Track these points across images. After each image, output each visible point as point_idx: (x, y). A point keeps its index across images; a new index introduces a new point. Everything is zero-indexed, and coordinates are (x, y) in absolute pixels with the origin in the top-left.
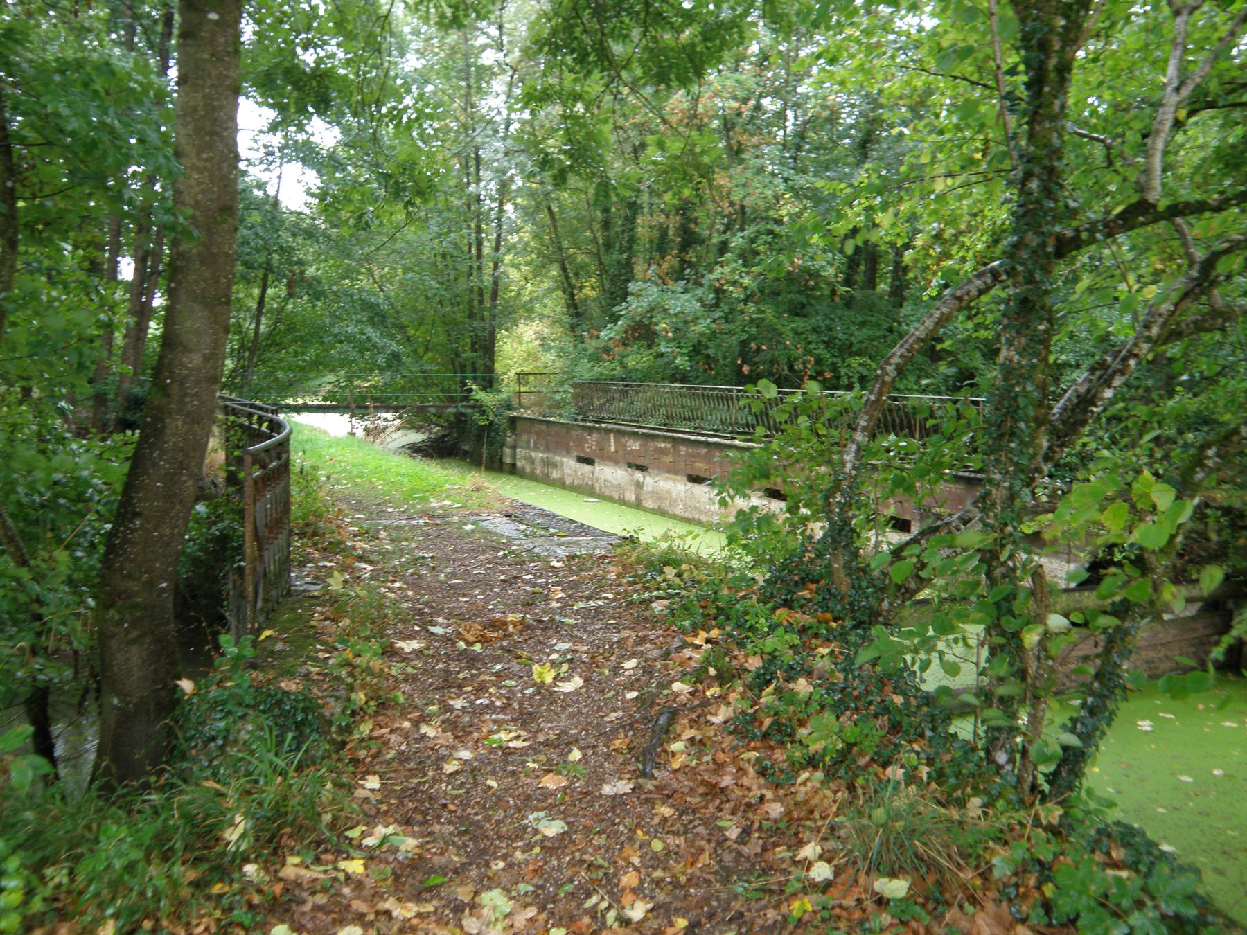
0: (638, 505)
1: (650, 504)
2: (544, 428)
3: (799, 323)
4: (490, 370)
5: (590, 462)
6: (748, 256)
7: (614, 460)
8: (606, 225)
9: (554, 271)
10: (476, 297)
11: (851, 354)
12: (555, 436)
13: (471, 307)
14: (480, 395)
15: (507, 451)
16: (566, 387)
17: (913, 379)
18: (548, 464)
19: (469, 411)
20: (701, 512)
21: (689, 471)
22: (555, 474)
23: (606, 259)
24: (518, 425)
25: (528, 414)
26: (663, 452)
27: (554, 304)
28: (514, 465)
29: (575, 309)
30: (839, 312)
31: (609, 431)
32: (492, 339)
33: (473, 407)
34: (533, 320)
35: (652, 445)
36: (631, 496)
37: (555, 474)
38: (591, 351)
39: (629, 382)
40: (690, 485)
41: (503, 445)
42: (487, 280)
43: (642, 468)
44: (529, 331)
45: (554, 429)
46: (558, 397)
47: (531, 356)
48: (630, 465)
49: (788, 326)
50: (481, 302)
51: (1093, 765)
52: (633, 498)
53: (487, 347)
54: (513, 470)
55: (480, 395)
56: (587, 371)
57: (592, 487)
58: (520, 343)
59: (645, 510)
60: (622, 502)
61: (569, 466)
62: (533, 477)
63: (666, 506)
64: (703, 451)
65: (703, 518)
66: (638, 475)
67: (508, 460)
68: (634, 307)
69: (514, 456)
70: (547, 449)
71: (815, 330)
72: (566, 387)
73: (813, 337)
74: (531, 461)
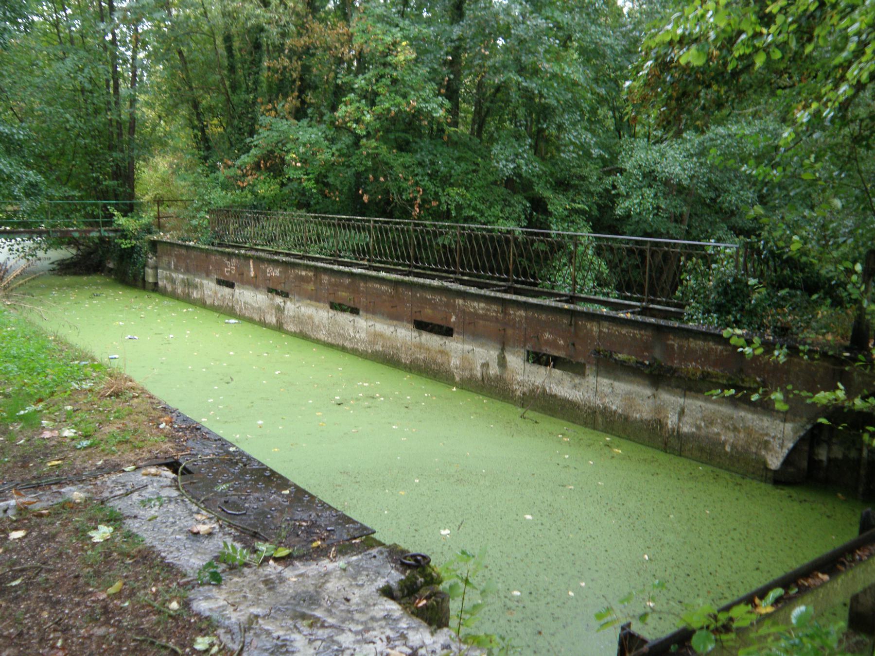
0: (279, 327)
1: (291, 328)
2: (184, 251)
3: (407, 159)
4: (132, 196)
5: (231, 285)
6: (371, 97)
7: (253, 284)
8: (232, 69)
9: (184, 111)
10: (116, 131)
11: (452, 185)
12: (195, 261)
13: (111, 139)
14: (121, 221)
15: (149, 271)
16: (203, 214)
17: (499, 207)
18: (188, 284)
19: (112, 235)
20: (343, 337)
21: (332, 299)
22: (195, 295)
23: (235, 99)
24: (159, 248)
25: (167, 237)
26: (303, 279)
27: (184, 138)
28: (156, 284)
29: (204, 143)
30: (440, 149)
31: (247, 258)
32: (131, 168)
33: (116, 231)
34: (166, 152)
35: (292, 272)
36: (272, 319)
37: (195, 295)
38: (221, 179)
39: (262, 208)
40: (332, 313)
41: (145, 265)
42: (125, 117)
43: (285, 295)
44: (162, 163)
45: (193, 254)
46: (194, 222)
47: (164, 181)
48: (270, 290)
49: (398, 161)
50: (120, 135)
51: (366, 320)
52: (274, 320)
53: (126, 176)
54: (155, 288)
55: (121, 221)
56: (219, 197)
57: (233, 308)
58: (156, 171)
59: (287, 333)
60: (263, 324)
61: (209, 288)
62: (174, 296)
63: (307, 330)
64: (347, 281)
65: (347, 344)
66: (279, 300)
67: (150, 279)
68: (262, 140)
69: (156, 275)
70: (187, 271)
71: (420, 164)
72: (203, 214)
73: (419, 170)
74: (173, 281)
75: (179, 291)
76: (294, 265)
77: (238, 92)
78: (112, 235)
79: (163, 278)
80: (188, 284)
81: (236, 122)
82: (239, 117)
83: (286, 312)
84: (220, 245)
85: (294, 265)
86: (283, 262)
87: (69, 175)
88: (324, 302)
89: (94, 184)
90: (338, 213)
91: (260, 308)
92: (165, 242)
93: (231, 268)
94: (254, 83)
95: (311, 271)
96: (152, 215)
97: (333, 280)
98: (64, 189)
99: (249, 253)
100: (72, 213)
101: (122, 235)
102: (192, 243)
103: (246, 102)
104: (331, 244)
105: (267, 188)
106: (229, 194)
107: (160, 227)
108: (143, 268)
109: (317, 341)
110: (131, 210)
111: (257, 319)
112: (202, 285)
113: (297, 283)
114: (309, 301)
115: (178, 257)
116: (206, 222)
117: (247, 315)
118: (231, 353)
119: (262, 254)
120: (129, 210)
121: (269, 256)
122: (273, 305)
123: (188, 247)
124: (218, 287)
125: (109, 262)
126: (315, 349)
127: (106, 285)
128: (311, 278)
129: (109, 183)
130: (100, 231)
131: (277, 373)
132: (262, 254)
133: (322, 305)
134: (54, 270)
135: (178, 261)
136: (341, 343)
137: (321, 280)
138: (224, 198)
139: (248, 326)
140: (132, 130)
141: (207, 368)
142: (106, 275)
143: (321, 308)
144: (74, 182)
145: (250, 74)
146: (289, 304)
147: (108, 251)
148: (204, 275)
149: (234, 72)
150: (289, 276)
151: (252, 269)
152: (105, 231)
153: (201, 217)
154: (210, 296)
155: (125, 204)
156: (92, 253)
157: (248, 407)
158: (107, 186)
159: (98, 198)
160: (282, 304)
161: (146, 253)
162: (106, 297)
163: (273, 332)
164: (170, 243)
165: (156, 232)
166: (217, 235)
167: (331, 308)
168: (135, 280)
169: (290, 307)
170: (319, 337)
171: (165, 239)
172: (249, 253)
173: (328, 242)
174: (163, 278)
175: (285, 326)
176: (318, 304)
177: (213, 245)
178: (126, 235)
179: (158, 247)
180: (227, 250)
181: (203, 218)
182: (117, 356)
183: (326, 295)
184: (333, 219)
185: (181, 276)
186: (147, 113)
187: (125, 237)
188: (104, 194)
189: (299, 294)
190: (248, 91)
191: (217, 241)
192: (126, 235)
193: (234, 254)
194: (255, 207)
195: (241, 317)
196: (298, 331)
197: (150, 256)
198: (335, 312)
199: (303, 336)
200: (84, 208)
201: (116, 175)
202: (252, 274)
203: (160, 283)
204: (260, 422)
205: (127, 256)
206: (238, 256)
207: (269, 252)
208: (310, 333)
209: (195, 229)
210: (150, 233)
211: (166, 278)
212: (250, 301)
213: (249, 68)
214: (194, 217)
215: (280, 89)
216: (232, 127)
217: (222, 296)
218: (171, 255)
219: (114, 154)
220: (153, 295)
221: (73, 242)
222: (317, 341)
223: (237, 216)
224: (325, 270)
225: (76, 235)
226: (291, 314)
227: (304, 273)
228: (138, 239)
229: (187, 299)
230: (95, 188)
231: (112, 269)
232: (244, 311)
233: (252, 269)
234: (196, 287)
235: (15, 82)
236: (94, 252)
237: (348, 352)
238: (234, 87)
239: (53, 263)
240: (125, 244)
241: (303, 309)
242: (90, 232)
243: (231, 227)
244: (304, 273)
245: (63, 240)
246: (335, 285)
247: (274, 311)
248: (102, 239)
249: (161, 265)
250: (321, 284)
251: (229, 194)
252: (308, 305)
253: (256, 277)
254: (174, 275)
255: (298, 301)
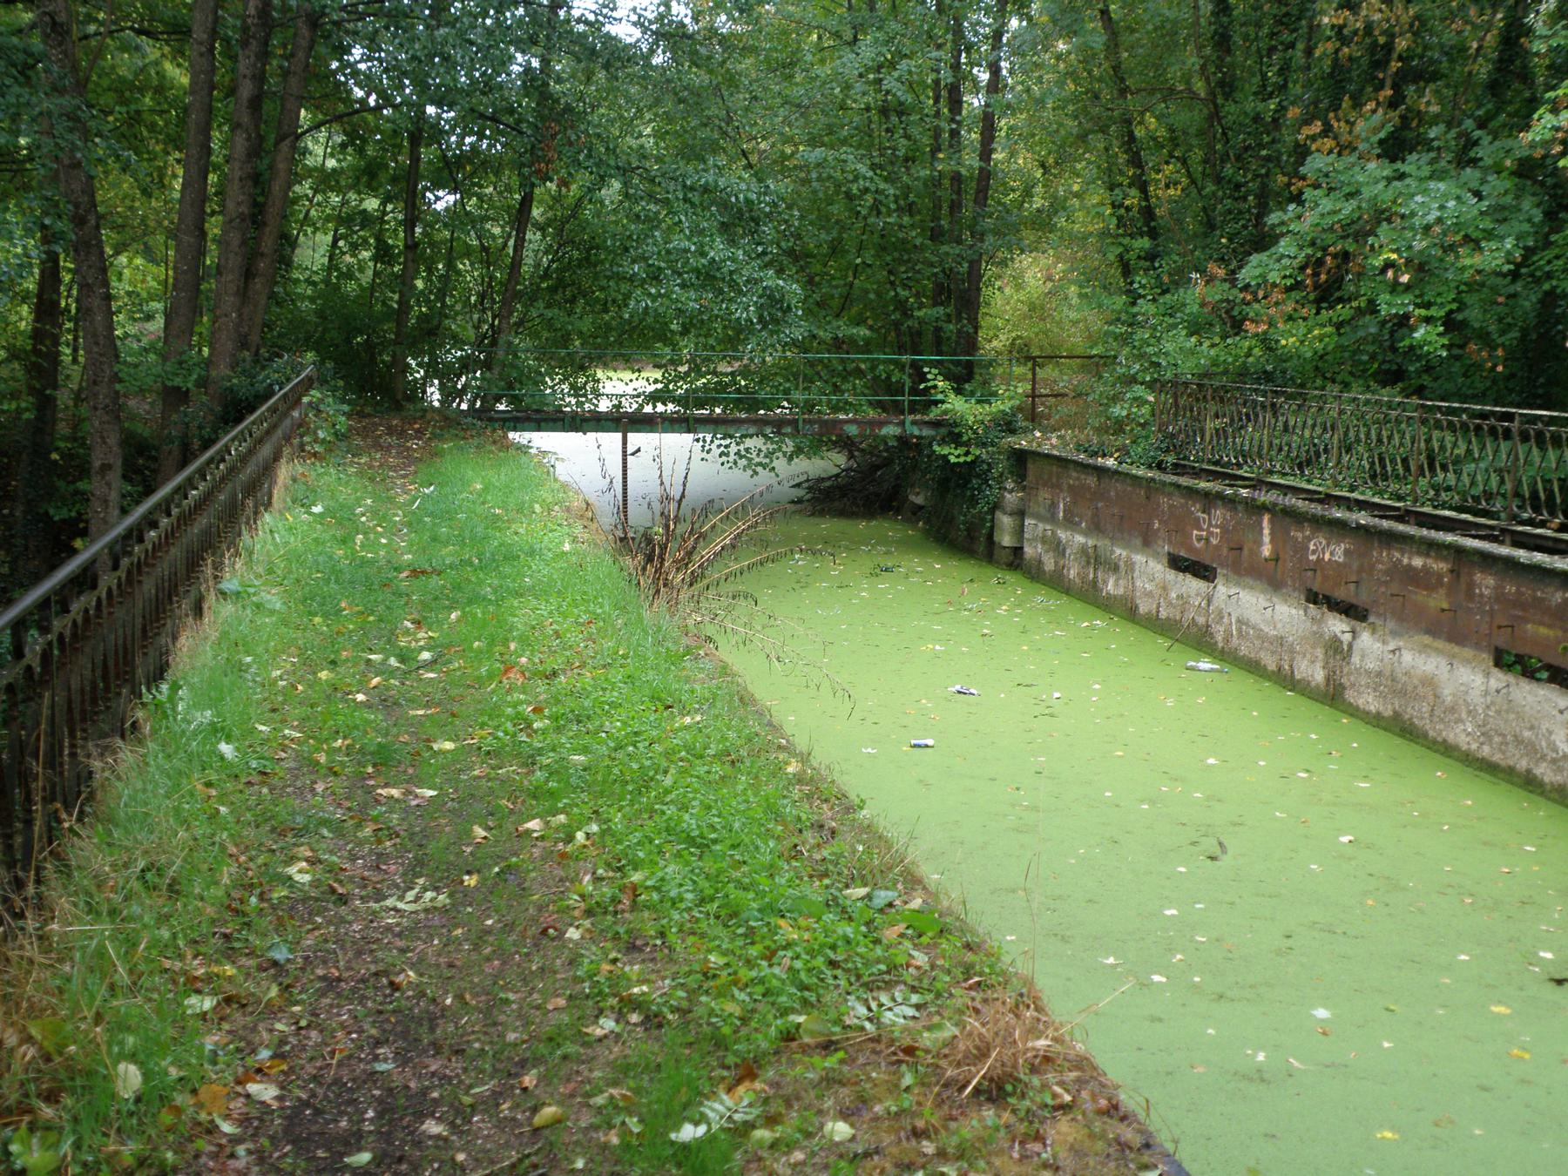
0: (1332, 696)
1: (1369, 701)
2: (1091, 481)
4: (971, 345)
5: (1202, 571)
7: (1270, 577)
8: (1222, 41)
12: (1118, 506)
14: (956, 405)
15: (1006, 521)
18: (1094, 559)
19: (927, 432)
20: (1531, 749)
21: (1501, 640)
22: (1112, 586)
25: (1051, 443)
28: (1018, 551)
31: (1256, 509)
32: (975, 276)
33: (936, 424)
35: (1384, 558)
39: (1279, 381)
40: (1498, 679)
41: (996, 507)
45: (1115, 488)
46: (1118, 411)
47: (1035, 310)
48: (1313, 598)
50: (955, 207)
52: (1319, 676)
53: (963, 296)
54: (1015, 560)
55: (956, 405)
56: (1185, 352)
57: (1206, 631)
60: (1286, 680)
61: (1148, 575)
62: (1057, 583)
63: (1417, 712)
65: (1543, 771)
66: (1337, 625)
67: (1007, 540)
69: (1020, 531)
70: (1096, 528)
74: (1059, 549)
75: (1073, 573)
76: (1390, 538)
77: (1238, 96)
78: (927, 432)
79: (1035, 539)
80: (1094, 559)
81: (1229, 170)
82: (1238, 158)
83: (1356, 659)
84: (1179, 469)
85: (1390, 538)
86: (1359, 527)
87: (847, 299)
88: (1477, 646)
89: (896, 316)
90: (1480, 398)
91: (1281, 640)
92: (1048, 456)
93: (1209, 531)
94: (1281, 72)
95: (1444, 559)
96: (1020, 390)
97: (1510, 589)
98: (835, 324)
99: (1264, 497)
100: (845, 379)
101: (951, 433)
102: (1110, 462)
103: (1257, 118)
104: (1466, 480)
105: (1301, 336)
106: (1206, 344)
107: (1033, 417)
108: (992, 511)
109: (1447, 750)
110: (969, 377)
111: (1272, 667)
112: (1131, 566)
113: (1395, 588)
114: (1427, 639)
115: (1076, 492)
116: (1145, 410)
117: (1244, 651)
118: (1211, 761)
119: (1291, 501)
120: (964, 376)
121: (1316, 509)
122: (1318, 635)
123: (1102, 471)
124: (1171, 575)
125: (916, 493)
126: (1441, 774)
127: (905, 545)
128: (1440, 576)
129: (927, 312)
130: (902, 423)
131: (1345, 839)
132: (1291, 501)
133: (1468, 652)
134: (800, 501)
135: (1074, 502)
136: (1522, 765)
137: (1471, 586)
138: (1192, 352)
139: (1245, 683)
140: (982, 194)
141: (1152, 802)
142: (906, 520)
143: (1467, 662)
144: (854, 310)
145: (1272, 50)
146: (1366, 639)
147: (914, 468)
148: (1138, 542)
149: (1228, 51)
150: (1372, 567)
151: (1266, 531)
152: (914, 423)
153: (1135, 399)
154: (1149, 594)
155: (958, 363)
156: (878, 467)
157: (1279, 952)
158: (921, 321)
159: (901, 349)
160: (1347, 637)
161: (1000, 479)
162: (907, 576)
163: (1316, 706)
164: (1058, 459)
165: (1025, 431)
166: (1172, 443)
167: (1498, 663)
168: (971, 536)
169: (1371, 647)
170: (1451, 738)
171: (1046, 449)
172: (1264, 497)
173: (1458, 473)
174: (1035, 539)
175: (1350, 695)
176: (1457, 649)
177: (1160, 466)
178: (960, 435)
179: (1030, 465)
180: (1203, 485)
181: (1140, 402)
182: (930, 742)
183: (1484, 628)
184: (1509, 417)
185: (1080, 539)
186: (1015, 160)
187: (955, 439)
188: (913, 341)
189: (1401, 619)
190: (1264, 94)
191: (1170, 459)
192: (960, 435)
193: (1220, 496)
194: (1268, 377)
195: (1227, 656)
196: (1388, 713)
197: (1010, 485)
198: (1511, 678)
199: (1402, 728)
200: (873, 368)
201: (941, 294)
202: (1266, 551)
203: (1029, 551)
204: (1322, 1013)
205: (960, 482)
206: (1231, 502)
207: (1311, 496)
208: (1424, 723)
209: (1119, 427)
210: (1013, 432)
211: (1044, 540)
212: (1254, 617)
213: (1272, 35)
214: (1115, 399)
215: (1340, 88)
216: (1218, 180)
217: (1180, 597)
218: (1059, 486)
219: (945, 248)
220: (1010, 577)
221: (846, 444)
222: (1447, 750)
223: (1220, 395)
224: (1487, 560)
225: (852, 430)
226: (1371, 665)
227: (1418, 562)
228: (984, 445)
229: (1090, 595)
230: (897, 325)
231: (921, 508)
232: (1235, 641)
233: (1267, 539)
234: (1115, 568)
235: (755, 98)
236: (887, 463)
237: (1542, 794)
238: (1227, 87)
239: (798, 485)
240: (955, 455)
241: (1407, 657)
242: (881, 424)
243: (1210, 425)
244: (1418, 562)
245: (827, 436)
246: (1517, 603)
247: (1320, 653)
248: (903, 440)
249: (1033, 507)
250: (1470, 595)
251: (1206, 344)
252: (1424, 649)
253: (1276, 559)
254: (1063, 535)
255: (1394, 634)
